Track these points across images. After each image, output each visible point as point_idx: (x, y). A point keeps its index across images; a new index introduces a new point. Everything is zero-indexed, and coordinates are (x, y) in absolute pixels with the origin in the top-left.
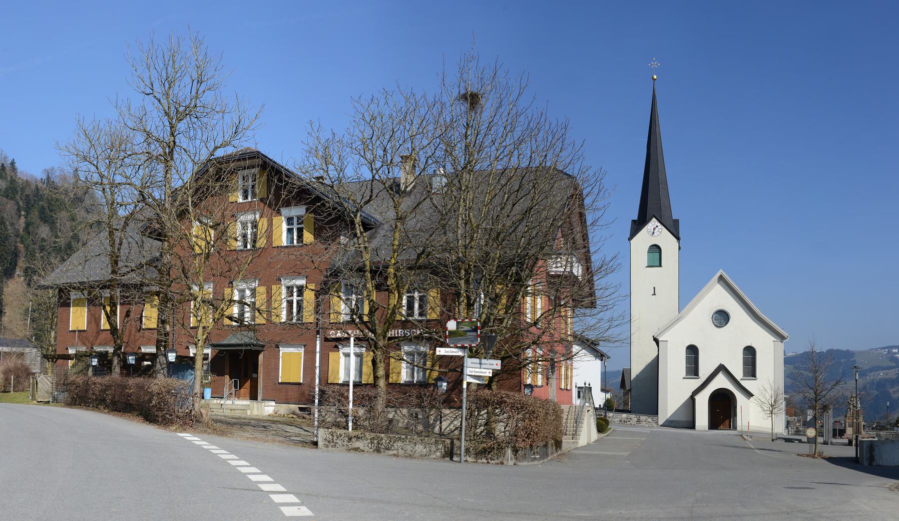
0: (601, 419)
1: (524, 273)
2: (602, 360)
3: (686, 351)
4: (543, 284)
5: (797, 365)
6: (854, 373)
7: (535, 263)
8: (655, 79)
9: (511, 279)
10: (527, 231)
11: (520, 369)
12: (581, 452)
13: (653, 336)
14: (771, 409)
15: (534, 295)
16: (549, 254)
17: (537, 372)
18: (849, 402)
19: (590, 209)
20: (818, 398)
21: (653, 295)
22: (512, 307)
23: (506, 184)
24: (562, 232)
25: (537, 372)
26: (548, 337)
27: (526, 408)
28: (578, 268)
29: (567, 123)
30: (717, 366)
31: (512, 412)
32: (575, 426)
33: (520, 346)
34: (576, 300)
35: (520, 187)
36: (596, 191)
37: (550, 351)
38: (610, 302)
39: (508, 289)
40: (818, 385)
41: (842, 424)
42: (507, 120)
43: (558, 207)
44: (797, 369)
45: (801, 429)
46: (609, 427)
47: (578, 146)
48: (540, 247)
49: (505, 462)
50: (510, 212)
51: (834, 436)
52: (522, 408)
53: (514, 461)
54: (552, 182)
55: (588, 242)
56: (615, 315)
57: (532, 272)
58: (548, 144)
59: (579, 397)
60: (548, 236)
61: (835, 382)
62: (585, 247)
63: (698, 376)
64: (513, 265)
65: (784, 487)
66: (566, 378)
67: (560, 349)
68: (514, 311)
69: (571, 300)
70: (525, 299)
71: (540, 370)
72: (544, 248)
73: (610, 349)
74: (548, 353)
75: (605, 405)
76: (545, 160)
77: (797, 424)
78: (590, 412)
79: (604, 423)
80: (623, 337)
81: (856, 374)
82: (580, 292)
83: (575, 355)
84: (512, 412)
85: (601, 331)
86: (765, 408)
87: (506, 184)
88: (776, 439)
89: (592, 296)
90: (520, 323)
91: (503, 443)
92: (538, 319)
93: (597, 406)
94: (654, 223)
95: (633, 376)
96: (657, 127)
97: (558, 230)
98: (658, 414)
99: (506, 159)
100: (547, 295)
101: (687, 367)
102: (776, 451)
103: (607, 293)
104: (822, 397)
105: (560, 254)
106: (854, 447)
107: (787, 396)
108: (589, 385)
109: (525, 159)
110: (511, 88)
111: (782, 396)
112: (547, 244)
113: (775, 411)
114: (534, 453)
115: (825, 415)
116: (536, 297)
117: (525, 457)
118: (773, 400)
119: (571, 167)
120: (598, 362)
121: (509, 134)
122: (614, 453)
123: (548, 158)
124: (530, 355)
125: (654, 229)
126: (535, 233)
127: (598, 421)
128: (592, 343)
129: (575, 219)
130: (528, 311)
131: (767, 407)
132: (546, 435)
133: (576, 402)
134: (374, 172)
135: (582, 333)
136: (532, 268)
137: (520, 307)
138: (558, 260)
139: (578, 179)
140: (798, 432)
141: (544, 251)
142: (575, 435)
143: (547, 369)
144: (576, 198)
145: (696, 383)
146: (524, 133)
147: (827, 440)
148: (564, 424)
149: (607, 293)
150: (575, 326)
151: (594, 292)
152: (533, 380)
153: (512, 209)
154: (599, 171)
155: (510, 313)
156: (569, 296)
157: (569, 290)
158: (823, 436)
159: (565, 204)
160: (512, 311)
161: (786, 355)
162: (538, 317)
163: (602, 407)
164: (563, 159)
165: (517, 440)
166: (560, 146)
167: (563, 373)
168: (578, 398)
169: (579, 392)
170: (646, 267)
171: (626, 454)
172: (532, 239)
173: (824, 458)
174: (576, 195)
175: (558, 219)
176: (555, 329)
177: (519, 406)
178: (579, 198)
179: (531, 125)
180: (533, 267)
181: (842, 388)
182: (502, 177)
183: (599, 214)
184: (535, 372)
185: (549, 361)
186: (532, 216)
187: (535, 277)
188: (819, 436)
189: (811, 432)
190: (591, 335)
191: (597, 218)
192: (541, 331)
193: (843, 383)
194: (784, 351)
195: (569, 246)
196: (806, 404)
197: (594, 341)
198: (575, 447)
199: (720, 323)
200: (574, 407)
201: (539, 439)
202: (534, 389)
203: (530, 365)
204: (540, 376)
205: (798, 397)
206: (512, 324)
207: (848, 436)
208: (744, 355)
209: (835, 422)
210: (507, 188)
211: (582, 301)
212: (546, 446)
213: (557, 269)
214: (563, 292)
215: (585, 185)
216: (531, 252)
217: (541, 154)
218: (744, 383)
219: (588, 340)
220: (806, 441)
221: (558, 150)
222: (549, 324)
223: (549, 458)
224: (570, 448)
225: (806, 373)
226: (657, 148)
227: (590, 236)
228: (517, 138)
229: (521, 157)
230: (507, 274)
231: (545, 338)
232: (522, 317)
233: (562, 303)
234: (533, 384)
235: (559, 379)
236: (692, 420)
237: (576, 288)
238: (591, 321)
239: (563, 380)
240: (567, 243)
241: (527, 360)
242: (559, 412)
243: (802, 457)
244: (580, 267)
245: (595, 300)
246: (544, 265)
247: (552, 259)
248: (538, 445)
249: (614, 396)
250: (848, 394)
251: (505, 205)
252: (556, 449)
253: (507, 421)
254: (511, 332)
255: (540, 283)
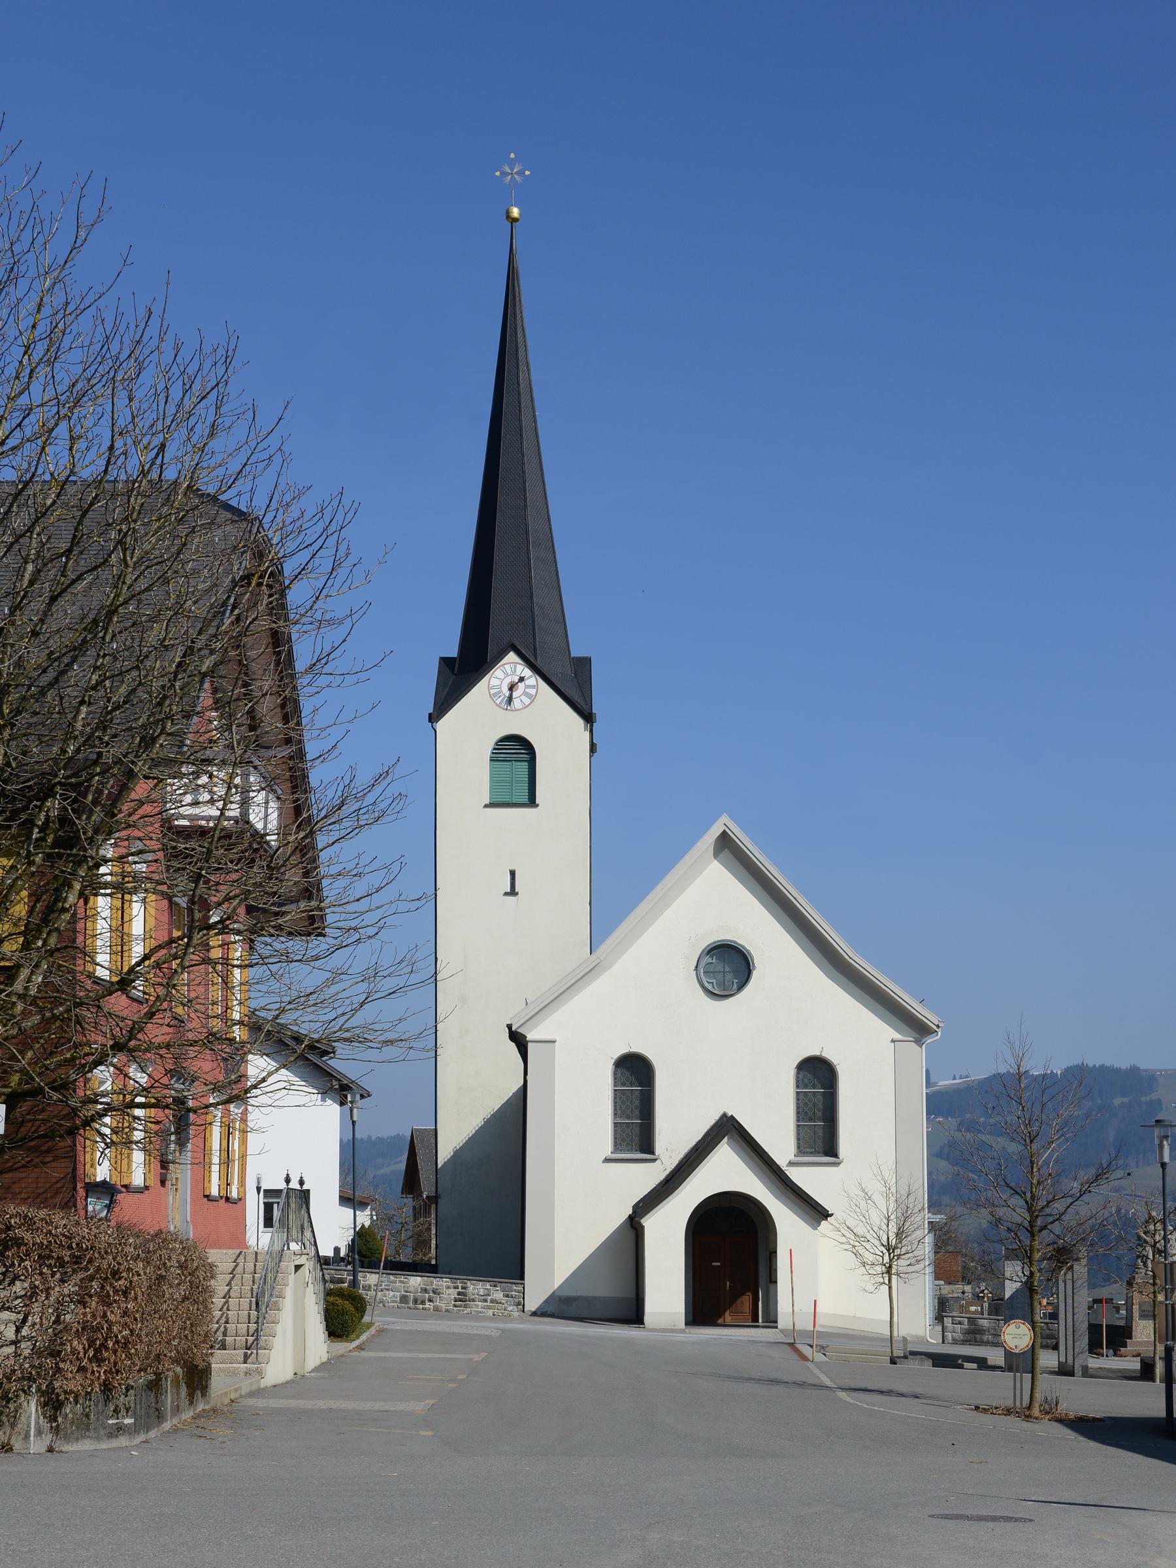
0: (340, 1293)
1: (88, 818)
2: (342, 1104)
3: (615, 1074)
4: (150, 857)
5: (968, 1116)
6: (1157, 1141)
7: (124, 789)
8: (515, 220)
9: (43, 839)
10: (97, 684)
11: (72, 1132)
12: (274, 1403)
13: (509, 1027)
14: (886, 1259)
15: (121, 889)
16: (170, 762)
17: (129, 1143)
18: (1139, 1238)
19: (304, 620)
20: (1039, 1222)
21: (506, 894)
22: (46, 930)
23: (30, 529)
24: (215, 691)
25: (129, 1143)
26: (166, 1029)
27: (90, 1261)
28: (266, 808)
29: (231, 347)
30: (712, 1122)
31: (41, 1274)
32: (253, 1319)
33: (73, 1058)
34: (256, 909)
35: (75, 541)
36: (324, 563)
37: (170, 1073)
38: (370, 918)
39: (33, 869)
40: (1039, 1183)
41: (1117, 1309)
42: (34, 327)
43: (201, 610)
44: (969, 1130)
45: (985, 1323)
46: (366, 1319)
47: (265, 421)
48: (142, 739)
49: (17, 1444)
50: (42, 621)
51: (1094, 1347)
52: (77, 1260)
53: (47, 1439)
54: (183, 530)
55: (299, 724)
56: (386, 961)
57: (114, 815)
58: (171, 409)
59: (268, 1222)
60: (167, 702)
61: (1093, 1171)
62: (288, 741)
63: (653, 1153)
64: (51, 793)
65: (932, 1516)
66: (227, 1161)
67: (207, 1066)
68: (53, 941)
69: (242, 911)
70: (90, 904)
71: (138, 1135)
72: (154, 740)
73: (370, 1066)
74: (165, 1081)
75: (351, 1247)
76: (159, 461)
77: (973, 1308)
78: (305, 1271)
79: (348, 1306)
80: (410, 1028)
81: (1161, 1146)
82: (271, 887)
83: (255, 1087)
84: (41, 1274)
85: (340, 1011)
86: (867, 1254)
87: (30, 529)
88: (905, 1357)
89: (310, 898)
90: (74, 983)
91: (9, 1379)
92: (132, 970)
93: (326, 1251)
94: (510, 667)
95: (445, 1153)
96: (522, 367)
97: (201, 685)
98: (522, 1277)
99: (31, 449)
100: (162, 893)
101: (616, 1125)
102: (902, 1395)
103: (360, 888)
104: (1051, 1219)
105: (208, 761)
106: (1159, 1386)
107: (937, 1218)
108: (301, 1182)
109: (92, 454)
110: (46, 224)
111: (922, 1218)
112: (164, 728)
113: (900, 1265)
114: (116, 1411)
115: (1061, 1279)
116: (127, 897)
117: (84, 1426)
118: (893, 1228)
119: (243, 485)
120: (332, 1111)
121: (42, 371)
122: (379, 1405)
123: (169, 453)
124: (107, 1086)
125: (512, 688)
126: (123, 690)
127: (331, 1299)
128: (312, 1047)
129: (258, 651)
130: (99, 943)
131: (874, 1252)
132: (156, 1349)
133: (259, 1238)
134: (157, 1084)
135: (277, 1017)
136: (114, 805)
137: (75, 931)
138: (200, 782)
139: (266, 526)
140: (974, 1335)
141: (155, 751)
142: (254, 1346)
143: (163, 1134)
144: (259, 585)
145: (647, 1177)
146: (92, 369)
147: (1070, 1361)
148: (217, 1314)
149: (360, 888)
150: (252, 995)
151: (319, 883)
152: (115, 1167)
153: (46, 613)
154: (335, 503)
155: (39, 948)
156: (236, 896)
157: (234, 876)
158: (1056, 1347)
159: (224, 604)
160: (45, 942)
161: (935, 1084)
162: (133, 962)
163: (342, 1254)
164: (218, 458)
165: (58, 1370)
166: (211, 418)
167: (216, 1146)
168: (266, 1226)
169: (268, 1208)
170: (486, 806)
171: (420, 1407)
172: (114, 709)
173: (1060, 1421)
174: (261, 577)
175: (200, 650)
176: (189, 1001)
177: (66, 1255)
178: (270, 587)
179: (115, 347)
180: (116, 799)
181: (1117, 1190)
182: (15, 509)
183: (332, 636)
184: (122, 1142)
185: (167, 1107)
186: (114, 636)
187: (124, 834)
188: (1042, 1347)
189: (1018, 1335)
190: (308, 1024)
191: (327, 650)
192: (145, 1009)
193: (1119, 1173)
194: (927, 1072)
195: (236, 737)
196: (1000, 1241)
197: (318, 1041)
198: (254, 1388)
199: (722, 985)
200: (251, 1258)
201: (135, 1365)
202: (119, 1197)
203: (107, 1120)
204: (138, 1157)
205: (974, 1222)
206: (45, 984)
207: (1140, 1349)
208: (798, 1087)
209: (1095, 1301)
210: (34, 544)
211: (276, 914)
212: (155, 1386)
213: (196, 811)
214: (218, 884)
215: (291, 546)
216: (111, 753)
217: (145, 441)
218: (796, 1175)
219: (298, 1039)
220: (1001, 1361)
221: (202, 430)
222: (170, 985)
223: (167, 1426)
224: (236, 1390)
225: (1000, 1143)
226: (521, 435)
227: (306, 706)
228: (67, 382)
229: (81, 445)
230: (29, 823)
231: (157, 1032)
232: (80, 962)
233: (214, 919)
234: (116, 1180)
235: (203, 1163)
236: (632, 1295)
237: (258, 873)
238: (306, 977)
239: (215, 1168)
240: (229, 728)
241: (97, 1102)
242: (201, 1274)
243: (987, 1418)
244: (271, 804)
245: (321, 909)
246: (154, 795)
247: (181, 776)
248: (131, 1382)
249: (385, 1218)
250: (1136, 1210)
251: (23, 598)
252: (191, 1395)
253: (26, 1305)
254: (41, 1011)
255: (140, 852)
